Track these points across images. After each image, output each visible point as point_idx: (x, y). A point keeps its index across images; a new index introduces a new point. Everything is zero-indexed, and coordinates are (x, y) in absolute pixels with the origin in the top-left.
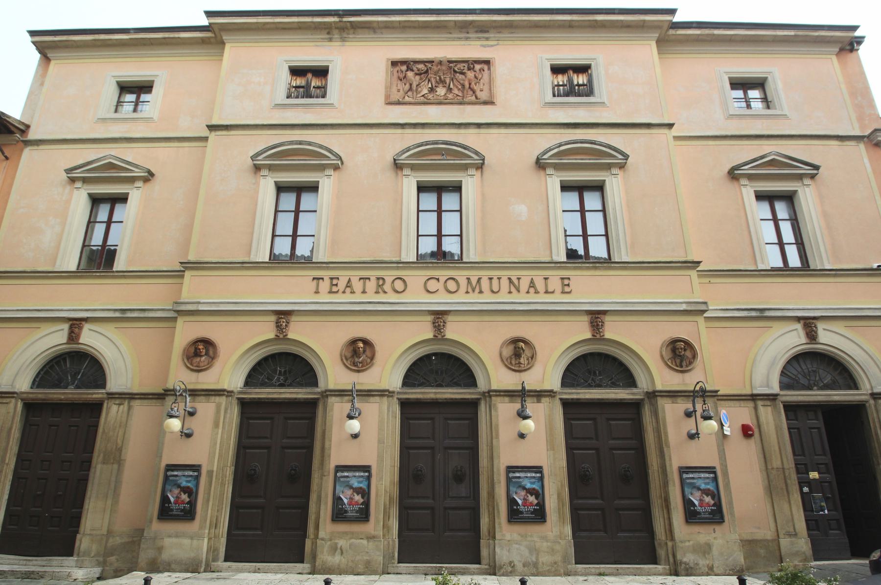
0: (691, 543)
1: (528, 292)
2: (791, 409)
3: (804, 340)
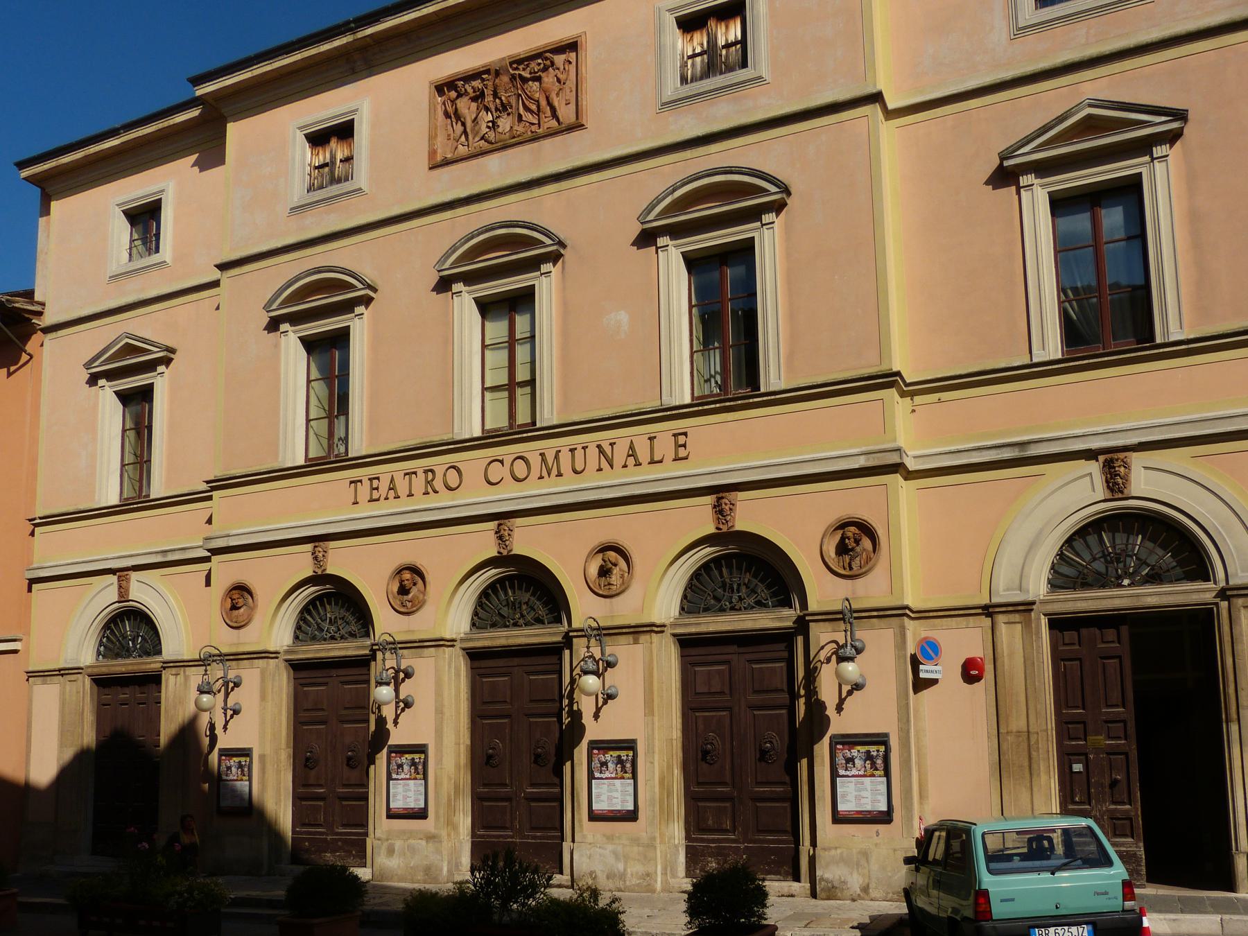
0: (839, 851)
1: (625, 466)
2: (1058, 624)
3: (1101, 492)
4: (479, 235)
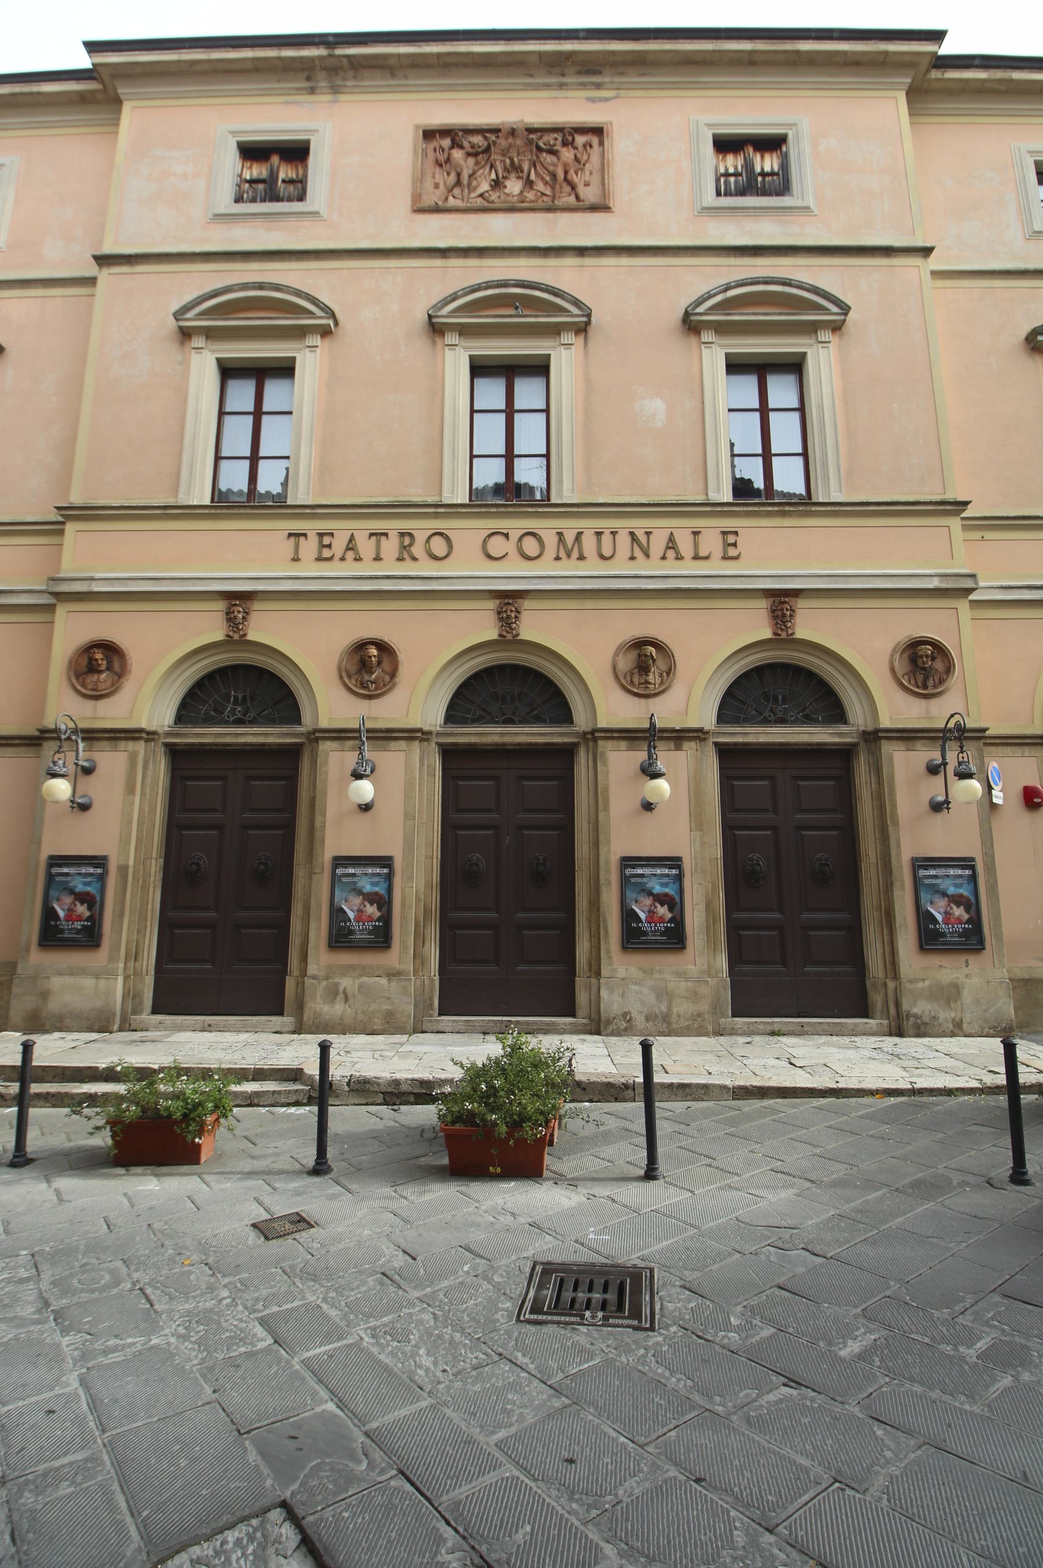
0: (927, 983)
1: (664, 558)
4: (487, 288)
